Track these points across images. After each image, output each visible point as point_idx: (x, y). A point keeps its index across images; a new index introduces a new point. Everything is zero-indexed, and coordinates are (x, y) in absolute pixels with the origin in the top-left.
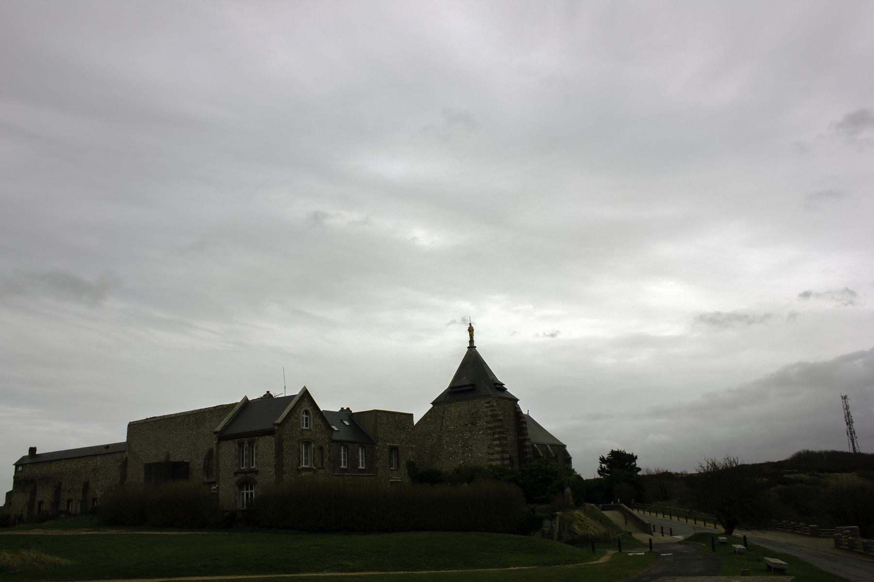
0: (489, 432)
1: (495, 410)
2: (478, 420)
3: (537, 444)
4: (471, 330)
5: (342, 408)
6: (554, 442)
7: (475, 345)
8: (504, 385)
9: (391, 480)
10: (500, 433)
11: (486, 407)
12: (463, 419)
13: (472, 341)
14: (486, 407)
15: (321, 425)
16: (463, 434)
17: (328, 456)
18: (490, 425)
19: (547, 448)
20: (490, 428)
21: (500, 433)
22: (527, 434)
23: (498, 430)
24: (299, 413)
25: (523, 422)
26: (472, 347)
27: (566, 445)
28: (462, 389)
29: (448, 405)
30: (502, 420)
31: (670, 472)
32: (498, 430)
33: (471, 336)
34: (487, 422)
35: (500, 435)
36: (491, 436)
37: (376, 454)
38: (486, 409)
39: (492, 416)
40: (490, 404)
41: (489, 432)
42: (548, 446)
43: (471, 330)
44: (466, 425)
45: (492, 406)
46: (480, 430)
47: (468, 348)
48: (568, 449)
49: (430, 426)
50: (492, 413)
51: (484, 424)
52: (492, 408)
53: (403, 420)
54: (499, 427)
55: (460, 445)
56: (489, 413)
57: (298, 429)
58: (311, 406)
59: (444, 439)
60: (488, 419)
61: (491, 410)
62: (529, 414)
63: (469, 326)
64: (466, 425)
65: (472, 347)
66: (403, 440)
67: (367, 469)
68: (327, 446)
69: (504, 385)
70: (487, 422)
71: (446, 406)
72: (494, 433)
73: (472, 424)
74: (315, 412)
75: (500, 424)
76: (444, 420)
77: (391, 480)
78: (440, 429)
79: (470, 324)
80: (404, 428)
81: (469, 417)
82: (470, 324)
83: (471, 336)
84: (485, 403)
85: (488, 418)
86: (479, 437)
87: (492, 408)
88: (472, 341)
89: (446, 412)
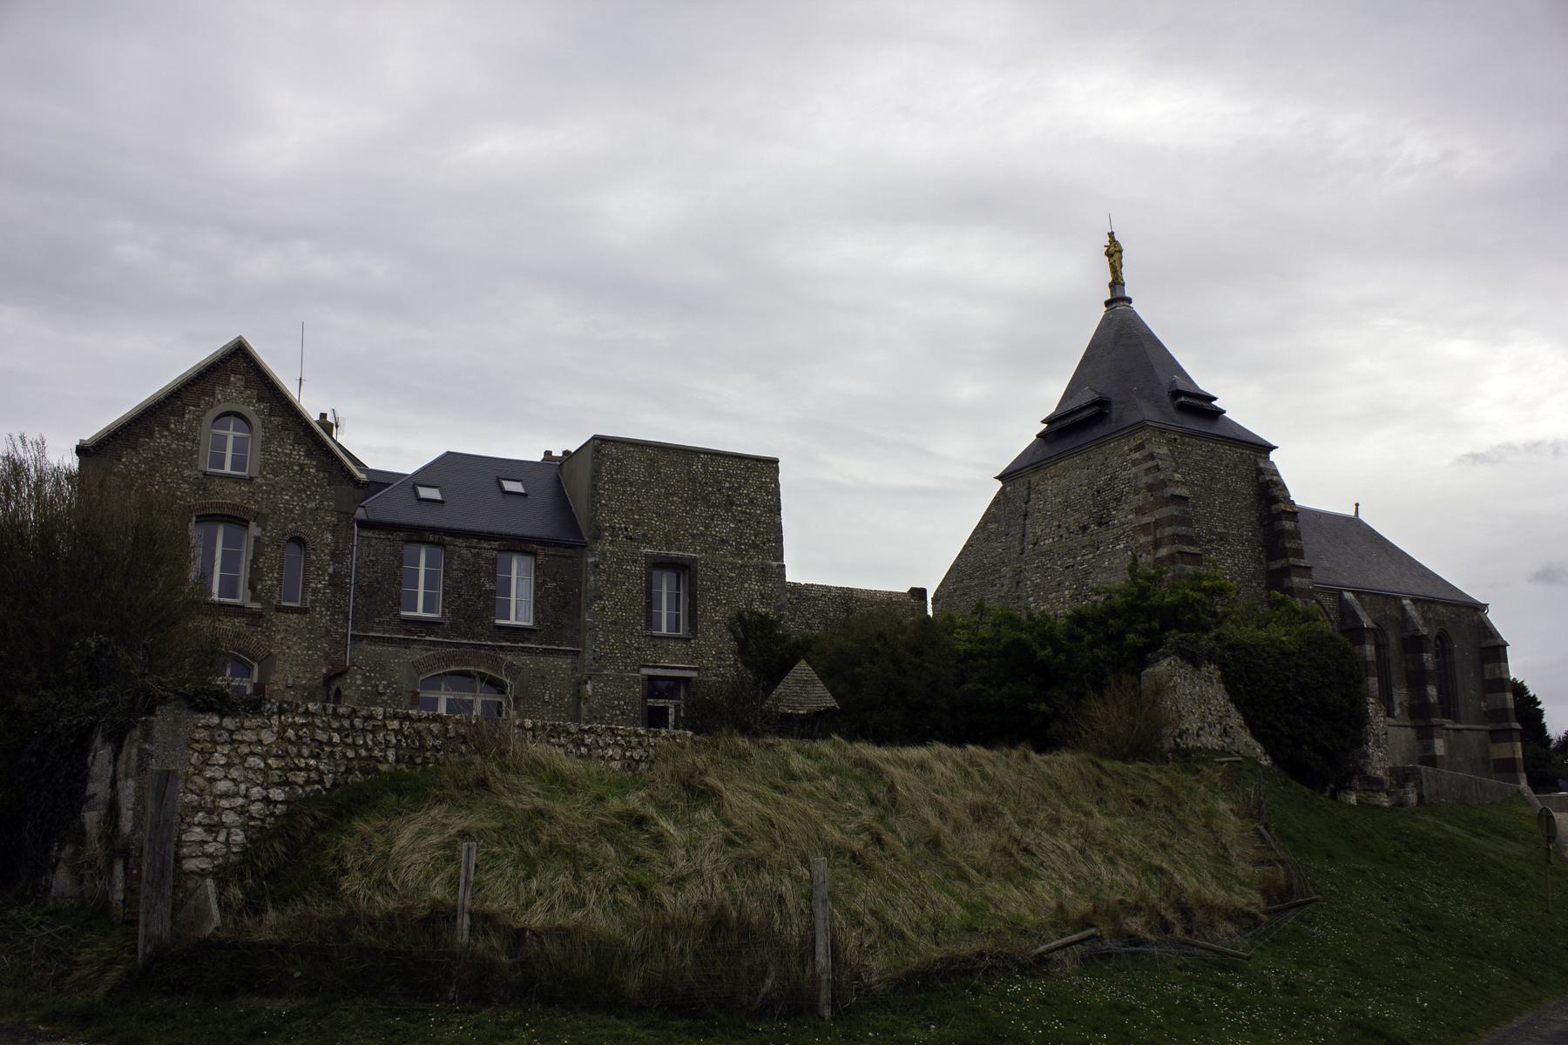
0: (1143, 540)
1: (1157, 467)
2: (1115, 509)
3: (1357, 593)
4: (1114, 252)
5: (548, 453)
6: (1432, 592)
7: (1128, 294)
8: (1215, 399)
9: (645, 671)
10: (1176, 538)
11: (1135, 463)
12: (1076, 511)
13: (1116, 283)
14: (1135, 463)
15: (302, 466)
16: (1075, 558)
17: (331, 570)
18: (1146, 520)
19: (1403, 609)
20: (1144, 529)
21: (1176, 538)
22: (1299, 553)
23: (1168, 531)
24: (199, 419)
25: (1285, 512)
26: (1117, 299)
27: (1486, 605)
28: (1078, 417)
29: (1037, 477)
30: (1186, 499)
31: (1544, 725)
32: (1168, 531)
33: (1116, 269)
34: (1139, 511)
35: (1179, 547)
36: (1148, 553)
37: (587, 580)
38: (1134, 470)
39: (1151, 488)
40: (1145, 452)
41: (1143, 540)
42: (1406, 602)
43: (1114, 252)
44: (1085, 528)
45: (1151, 457)
46: (1118, 539)
47: (1107, 303)
48: (1494, 617)
49: (995, 544)
50: (1149, 479)
51: (1130, 517)
52: (1150, 464)
53: (728, 475)
54: (1172, 520)
55: (1067, 592)
56: (1146, 480)
57: (186, 472)
58: (259, 400)
59: (1029, 579)
60: (1138, 500)
61: (1148, 471)
62: (1360, 517)
63: (1106, 241)
64: (1085, 528)
65: (1117, 299)
66: (723, 541)
67: (535, 628)
68: (329, 537)
69: (1215, 399)
70: (1139, 511)
71: (1034, 479)
72: (1157, 544)
73: (1100, 525)
74: (277, 420)
75: (1173, 510)
76: (1028, 522)
77: (645, 671)
78: (1018, 549)
79: (1111, 235)
80: (732, 504)
81: (1090, 502)
82: (1111, 235)
83: (1116, 269)
84: (1131, 450)
85: (1140, 496)
86: (1117, 561)
87: (1150, 464)
88: (1116, 283)
89: (1033, 496)
